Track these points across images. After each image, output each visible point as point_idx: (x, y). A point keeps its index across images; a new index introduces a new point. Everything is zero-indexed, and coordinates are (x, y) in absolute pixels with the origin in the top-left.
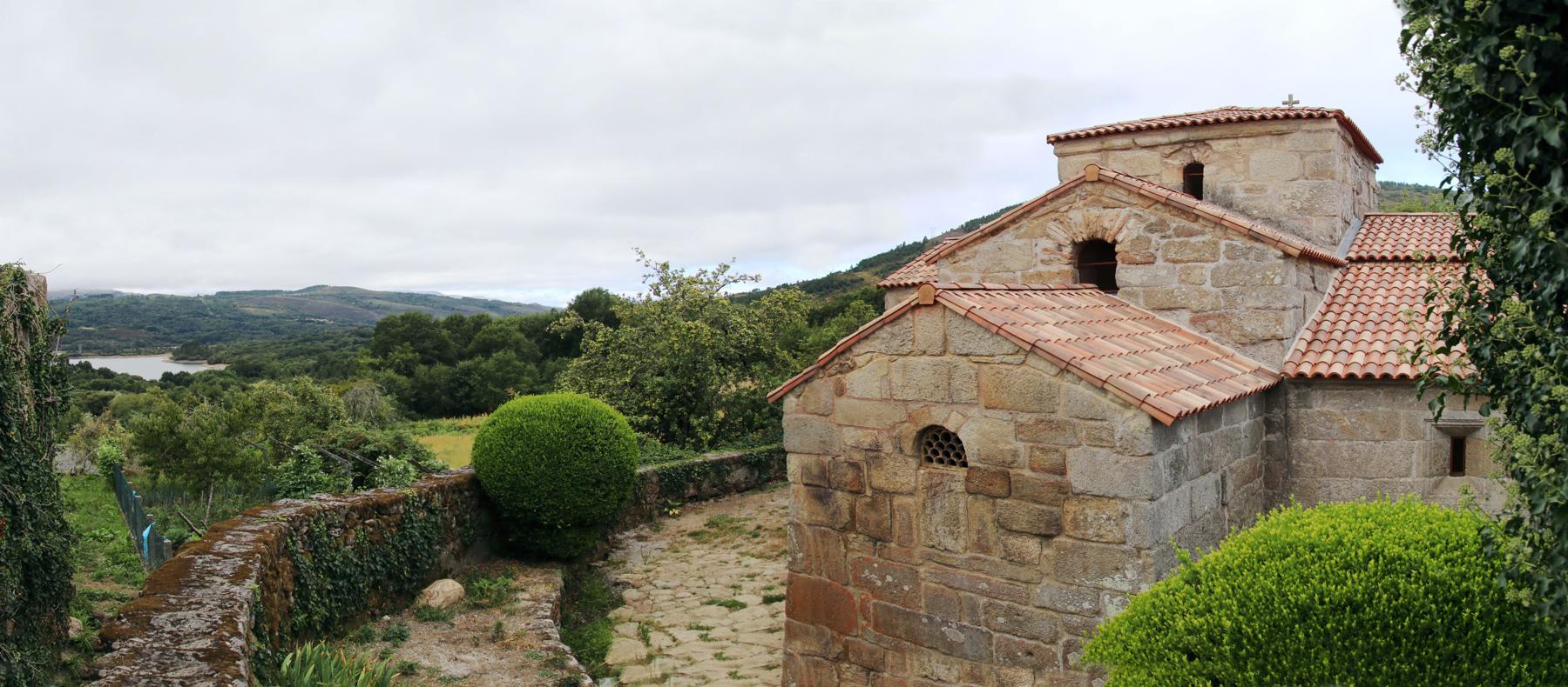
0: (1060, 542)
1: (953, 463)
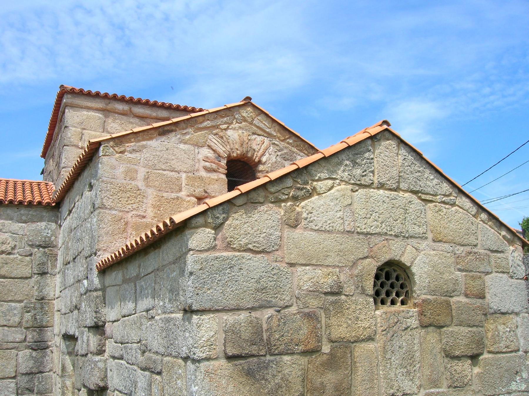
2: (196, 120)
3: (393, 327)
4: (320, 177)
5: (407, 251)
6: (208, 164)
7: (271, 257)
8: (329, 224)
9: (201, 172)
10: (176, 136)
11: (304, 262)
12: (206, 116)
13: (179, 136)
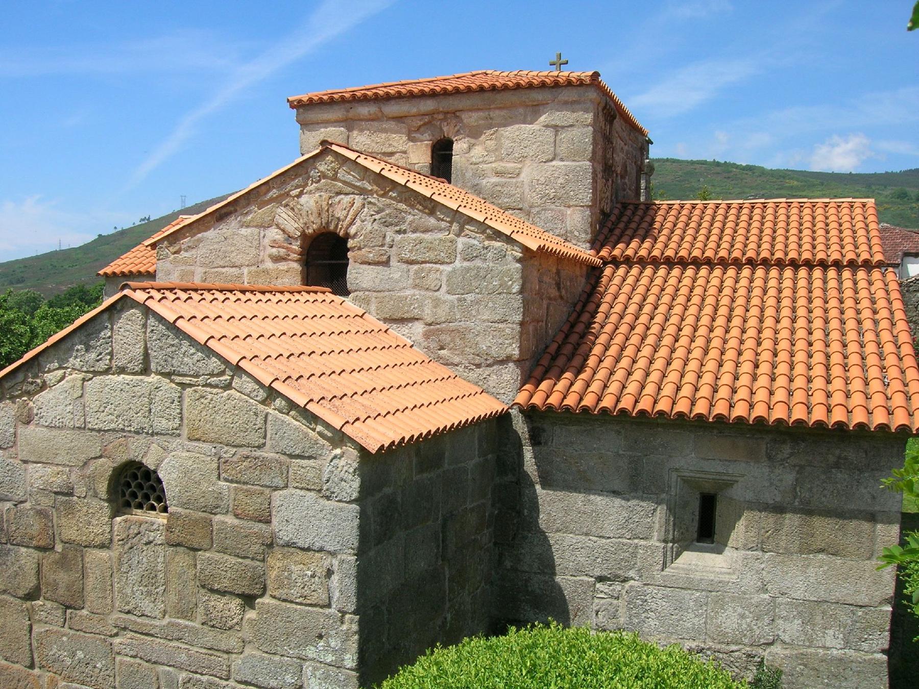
0: (263, 604)
1: (153, 508)
2: (258, 191)
3: (134, 538)
4: (49, 368)
5: (151, 452)
6: (274, 251)
7: (7, 453)
8: (59, 419)
9: (266, 263)
10: (236, 219)
11: (34, 460)
12: (270, 183)
13: (239, 219)
